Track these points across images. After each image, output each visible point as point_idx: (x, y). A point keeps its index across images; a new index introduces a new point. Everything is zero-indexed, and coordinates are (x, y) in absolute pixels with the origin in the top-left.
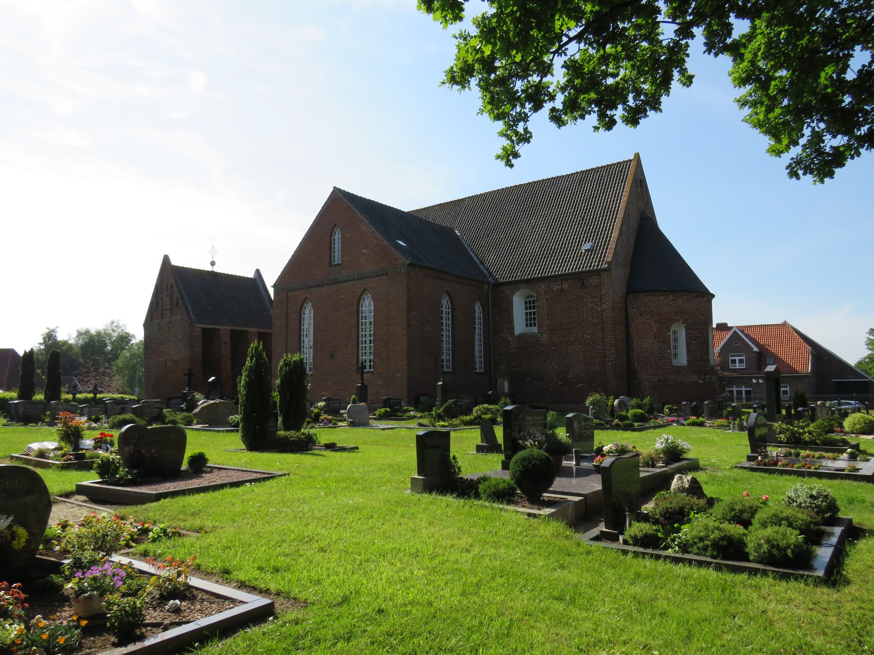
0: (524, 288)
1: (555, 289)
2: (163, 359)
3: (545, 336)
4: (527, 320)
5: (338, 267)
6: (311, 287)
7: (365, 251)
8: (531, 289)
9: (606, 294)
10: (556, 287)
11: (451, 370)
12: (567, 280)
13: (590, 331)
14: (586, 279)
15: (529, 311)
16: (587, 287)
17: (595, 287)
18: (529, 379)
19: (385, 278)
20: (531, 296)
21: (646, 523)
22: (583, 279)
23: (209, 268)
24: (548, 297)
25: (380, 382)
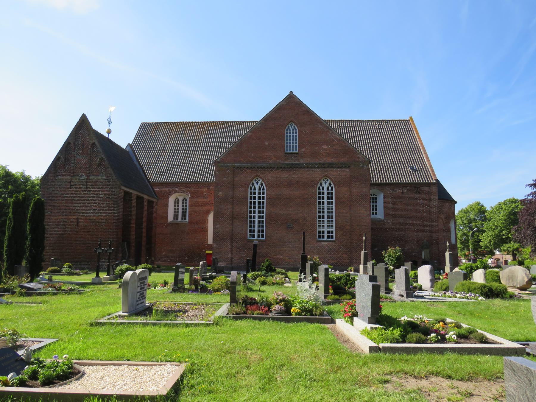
0: (375, 189)
1: (397, 192)
2: (75, 217)
3: (389, 221)
4: (376, 210)
5: (295, 155)
6: (264, 167)
7: (325, 147)
8: (380, 190)
9: (434, 198)
10: (399, 191)
11: (264, 239)
12: (407, 187)
13: (421, 221)
14: (419, 188)
15: (374, 204)
16: (420, 193)
17: (426, 193)
18: (377, 249)
19: (347, 170)
20: (374, 195)
21: (141, 316)
22: (417, 188)
23: (106, 135)
24: (392, 196)
25: (342, 249)
